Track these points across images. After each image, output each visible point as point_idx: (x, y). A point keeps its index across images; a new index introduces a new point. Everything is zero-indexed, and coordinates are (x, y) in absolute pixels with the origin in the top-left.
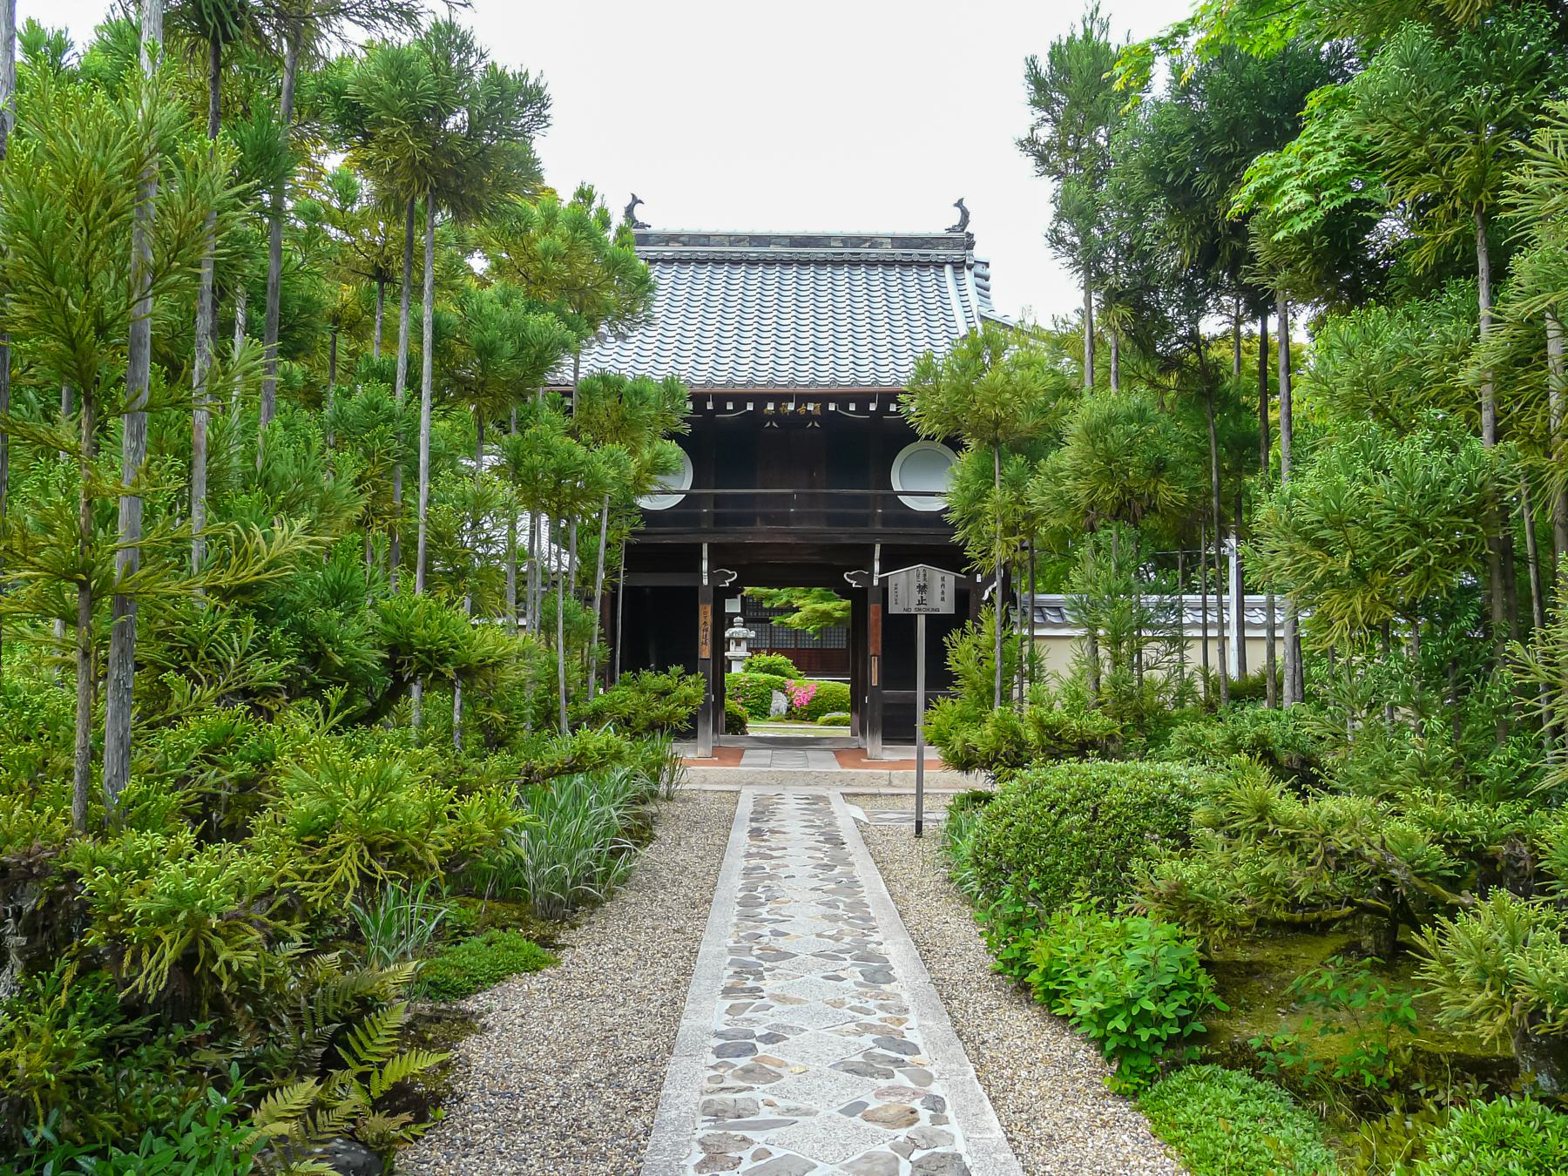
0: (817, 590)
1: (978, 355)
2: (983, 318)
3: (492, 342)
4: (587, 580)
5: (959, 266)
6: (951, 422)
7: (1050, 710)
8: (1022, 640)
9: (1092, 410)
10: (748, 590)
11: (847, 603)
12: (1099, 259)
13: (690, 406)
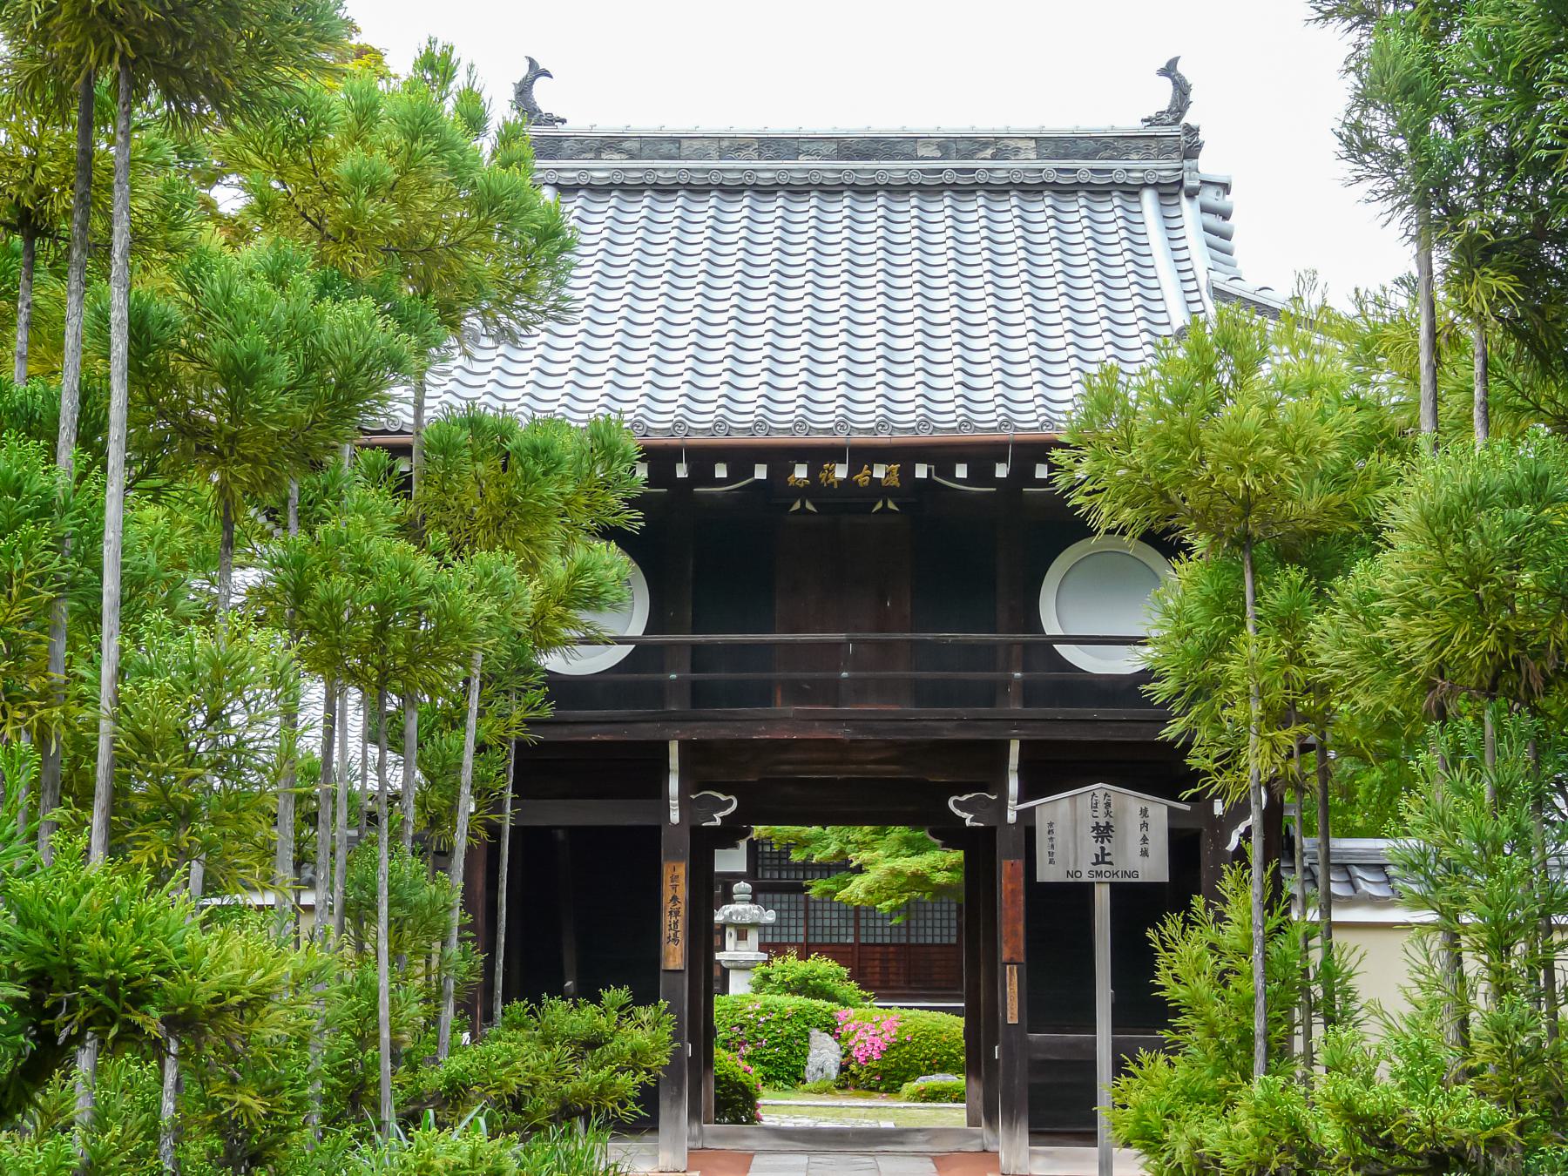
0: (898, 832)
1: (1209, 371)
2: (1220, 294)
3: (252, 358)
4: (437, 819)
5: (1169, 191)
6: (1155, 502)
7: (1368, 1082)
8: (1308, 937)
9: (1438, 478)
10: (759, 831)
11: (956, 856)
12: (1444, 183)
13: (642, 472)
